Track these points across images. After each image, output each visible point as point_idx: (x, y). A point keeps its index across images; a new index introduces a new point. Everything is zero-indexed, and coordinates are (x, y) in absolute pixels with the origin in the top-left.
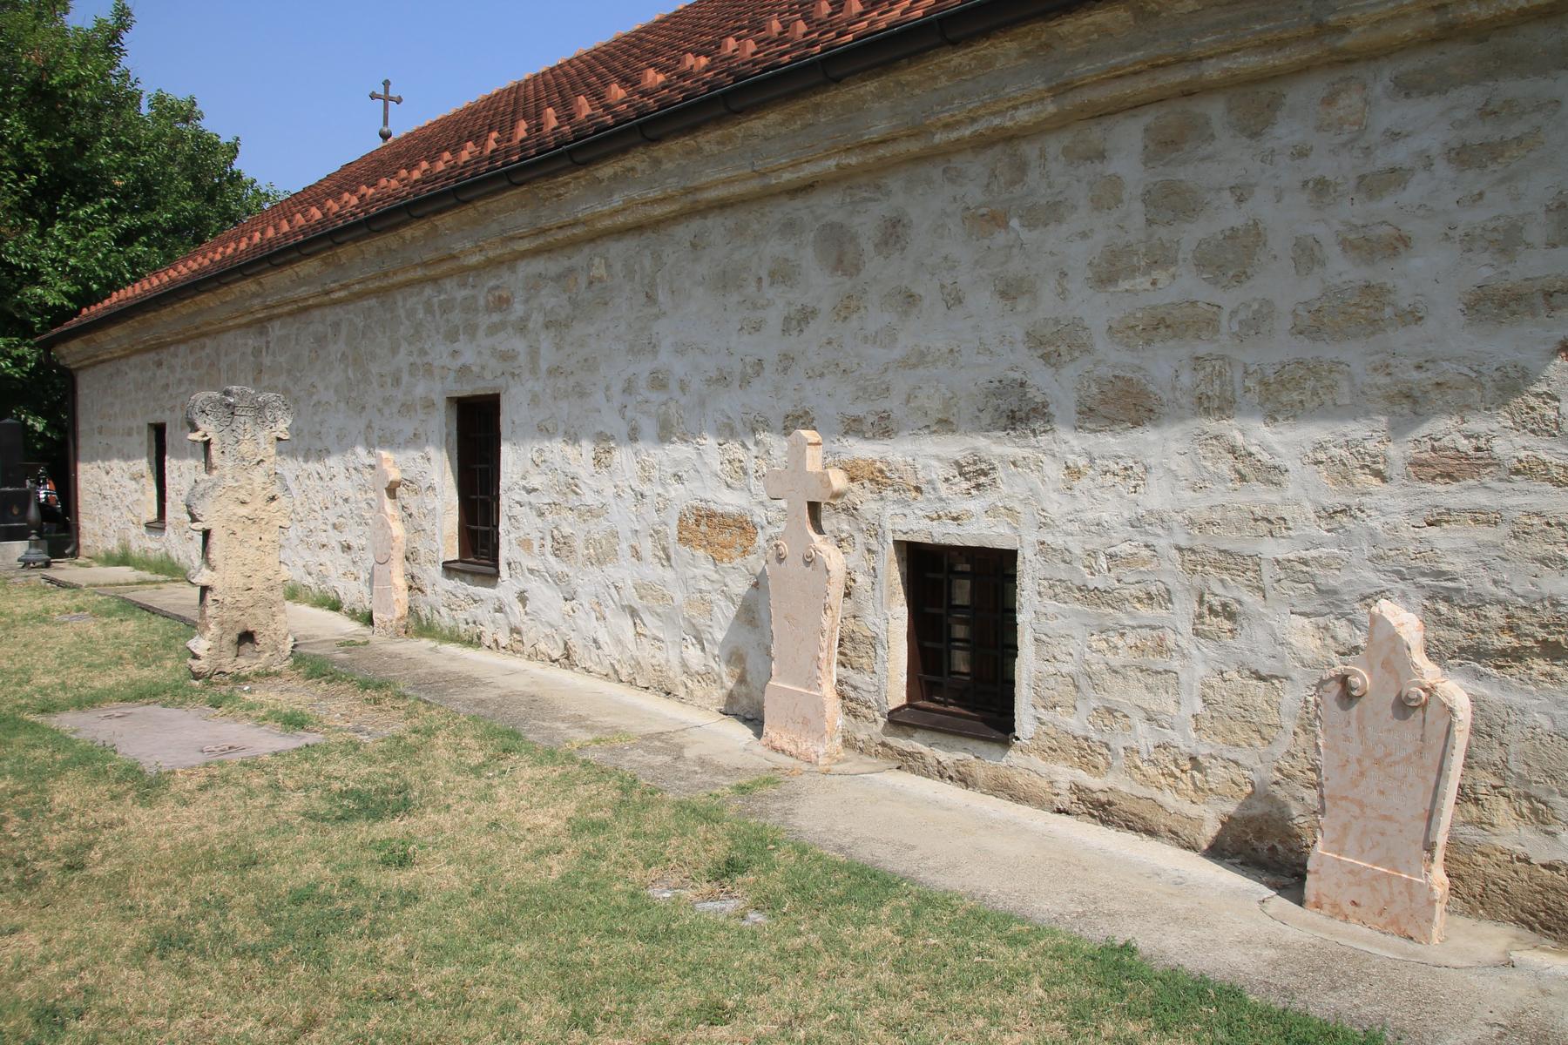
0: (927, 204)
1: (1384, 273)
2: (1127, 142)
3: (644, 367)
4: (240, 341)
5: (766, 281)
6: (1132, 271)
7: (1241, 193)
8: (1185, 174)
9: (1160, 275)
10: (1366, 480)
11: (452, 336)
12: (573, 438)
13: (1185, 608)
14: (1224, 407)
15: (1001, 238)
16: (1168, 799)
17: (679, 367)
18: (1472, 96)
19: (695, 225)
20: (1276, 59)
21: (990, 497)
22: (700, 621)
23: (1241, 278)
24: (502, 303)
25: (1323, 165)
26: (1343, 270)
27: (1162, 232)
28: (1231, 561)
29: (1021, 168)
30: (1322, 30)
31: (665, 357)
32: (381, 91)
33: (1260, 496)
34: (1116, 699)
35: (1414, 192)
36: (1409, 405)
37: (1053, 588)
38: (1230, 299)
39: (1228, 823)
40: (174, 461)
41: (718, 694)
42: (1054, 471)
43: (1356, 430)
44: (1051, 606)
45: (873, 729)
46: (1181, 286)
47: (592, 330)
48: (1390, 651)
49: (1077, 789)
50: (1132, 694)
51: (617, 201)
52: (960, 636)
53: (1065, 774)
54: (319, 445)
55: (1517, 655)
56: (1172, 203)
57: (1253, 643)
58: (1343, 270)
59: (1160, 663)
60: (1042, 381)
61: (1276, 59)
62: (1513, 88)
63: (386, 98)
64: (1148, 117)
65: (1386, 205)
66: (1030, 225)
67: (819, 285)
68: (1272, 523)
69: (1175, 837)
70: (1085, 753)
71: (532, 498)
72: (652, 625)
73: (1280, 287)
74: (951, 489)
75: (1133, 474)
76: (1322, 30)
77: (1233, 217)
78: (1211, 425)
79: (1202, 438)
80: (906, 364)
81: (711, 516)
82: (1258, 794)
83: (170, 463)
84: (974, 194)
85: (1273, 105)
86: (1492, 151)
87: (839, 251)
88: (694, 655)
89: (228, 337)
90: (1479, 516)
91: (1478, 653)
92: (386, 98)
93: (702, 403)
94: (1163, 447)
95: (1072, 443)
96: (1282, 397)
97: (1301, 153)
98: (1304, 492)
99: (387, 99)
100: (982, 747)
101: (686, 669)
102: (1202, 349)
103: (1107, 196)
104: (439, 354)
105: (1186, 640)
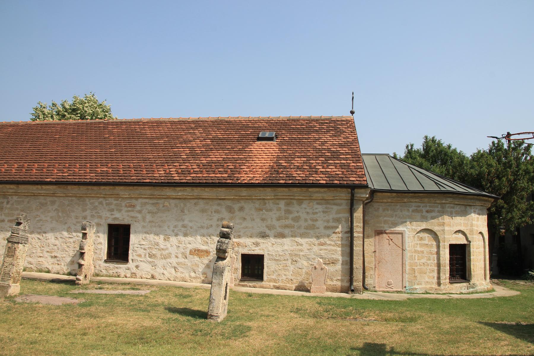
0: (248, 206)
1: (315, 223)
2: (282, 204)
3: (180, 224)
5: (213, 212)
6: (282, 219)
7: (298, 212)
8: (290, 208)
10: (313, 245)
12: (157, 234)
13: (290, 261)
14: (295, 236)
15: (261, 212)
16: (288, 285)
17: (190, 224)
18: (324, 206)
19: (196, 201)
20: (304, 198)
21: (259, 247)
22: (195, 268)
23: (298, 222)
25: (308, 210)
26: (310, 222)
27: (287, 215)
29: (265, 204)
30: (310, 196)
31: (186, 222)
35: (318, 215)
36: (318, 237)
38: (296, 224)
41: (199, 280)
43: (311, 240)
44: (270, 262)
45: (237, 282)
46: (289, 222)
47: (115, 202)
49: (274, 286)
51: (180, 194)
52: (253, 267)
53: (272, 284)
54: (39, 231)
55: (329, 264)
56: (288, 212)
57: (299, 265)
58: (310, 222)
59: (286, 268)
60: (268, 232)
61: (304, 198)
62: (328, 206)
64: (285, 201)
65: (315, 216)
66: (267, 211)
68: (301, 250)
69: (289, 289)
70: (275, 281)
71: (142, 246)
72: (181, 269)
73: (302, 223)
75: (282, 245)
76: (310, 196)
77: (296, 214)
78: (293, 239)
79: (292, 240)
80: (243, 228)
81: (198, 250)
82: (301, 282)
83: (365, 240)
84: (257, 206)
85: (302, 203)
87: (230, 210)
88: (193, 274)
93: (196, 231)
94: (287, 241)
95: (273, 240)
96: (302, 236)
98: (305, 247)
101: (190, 276)
102: (292, 230)
103: (279, 209)
104: (105, 214)
105: (290, 265)
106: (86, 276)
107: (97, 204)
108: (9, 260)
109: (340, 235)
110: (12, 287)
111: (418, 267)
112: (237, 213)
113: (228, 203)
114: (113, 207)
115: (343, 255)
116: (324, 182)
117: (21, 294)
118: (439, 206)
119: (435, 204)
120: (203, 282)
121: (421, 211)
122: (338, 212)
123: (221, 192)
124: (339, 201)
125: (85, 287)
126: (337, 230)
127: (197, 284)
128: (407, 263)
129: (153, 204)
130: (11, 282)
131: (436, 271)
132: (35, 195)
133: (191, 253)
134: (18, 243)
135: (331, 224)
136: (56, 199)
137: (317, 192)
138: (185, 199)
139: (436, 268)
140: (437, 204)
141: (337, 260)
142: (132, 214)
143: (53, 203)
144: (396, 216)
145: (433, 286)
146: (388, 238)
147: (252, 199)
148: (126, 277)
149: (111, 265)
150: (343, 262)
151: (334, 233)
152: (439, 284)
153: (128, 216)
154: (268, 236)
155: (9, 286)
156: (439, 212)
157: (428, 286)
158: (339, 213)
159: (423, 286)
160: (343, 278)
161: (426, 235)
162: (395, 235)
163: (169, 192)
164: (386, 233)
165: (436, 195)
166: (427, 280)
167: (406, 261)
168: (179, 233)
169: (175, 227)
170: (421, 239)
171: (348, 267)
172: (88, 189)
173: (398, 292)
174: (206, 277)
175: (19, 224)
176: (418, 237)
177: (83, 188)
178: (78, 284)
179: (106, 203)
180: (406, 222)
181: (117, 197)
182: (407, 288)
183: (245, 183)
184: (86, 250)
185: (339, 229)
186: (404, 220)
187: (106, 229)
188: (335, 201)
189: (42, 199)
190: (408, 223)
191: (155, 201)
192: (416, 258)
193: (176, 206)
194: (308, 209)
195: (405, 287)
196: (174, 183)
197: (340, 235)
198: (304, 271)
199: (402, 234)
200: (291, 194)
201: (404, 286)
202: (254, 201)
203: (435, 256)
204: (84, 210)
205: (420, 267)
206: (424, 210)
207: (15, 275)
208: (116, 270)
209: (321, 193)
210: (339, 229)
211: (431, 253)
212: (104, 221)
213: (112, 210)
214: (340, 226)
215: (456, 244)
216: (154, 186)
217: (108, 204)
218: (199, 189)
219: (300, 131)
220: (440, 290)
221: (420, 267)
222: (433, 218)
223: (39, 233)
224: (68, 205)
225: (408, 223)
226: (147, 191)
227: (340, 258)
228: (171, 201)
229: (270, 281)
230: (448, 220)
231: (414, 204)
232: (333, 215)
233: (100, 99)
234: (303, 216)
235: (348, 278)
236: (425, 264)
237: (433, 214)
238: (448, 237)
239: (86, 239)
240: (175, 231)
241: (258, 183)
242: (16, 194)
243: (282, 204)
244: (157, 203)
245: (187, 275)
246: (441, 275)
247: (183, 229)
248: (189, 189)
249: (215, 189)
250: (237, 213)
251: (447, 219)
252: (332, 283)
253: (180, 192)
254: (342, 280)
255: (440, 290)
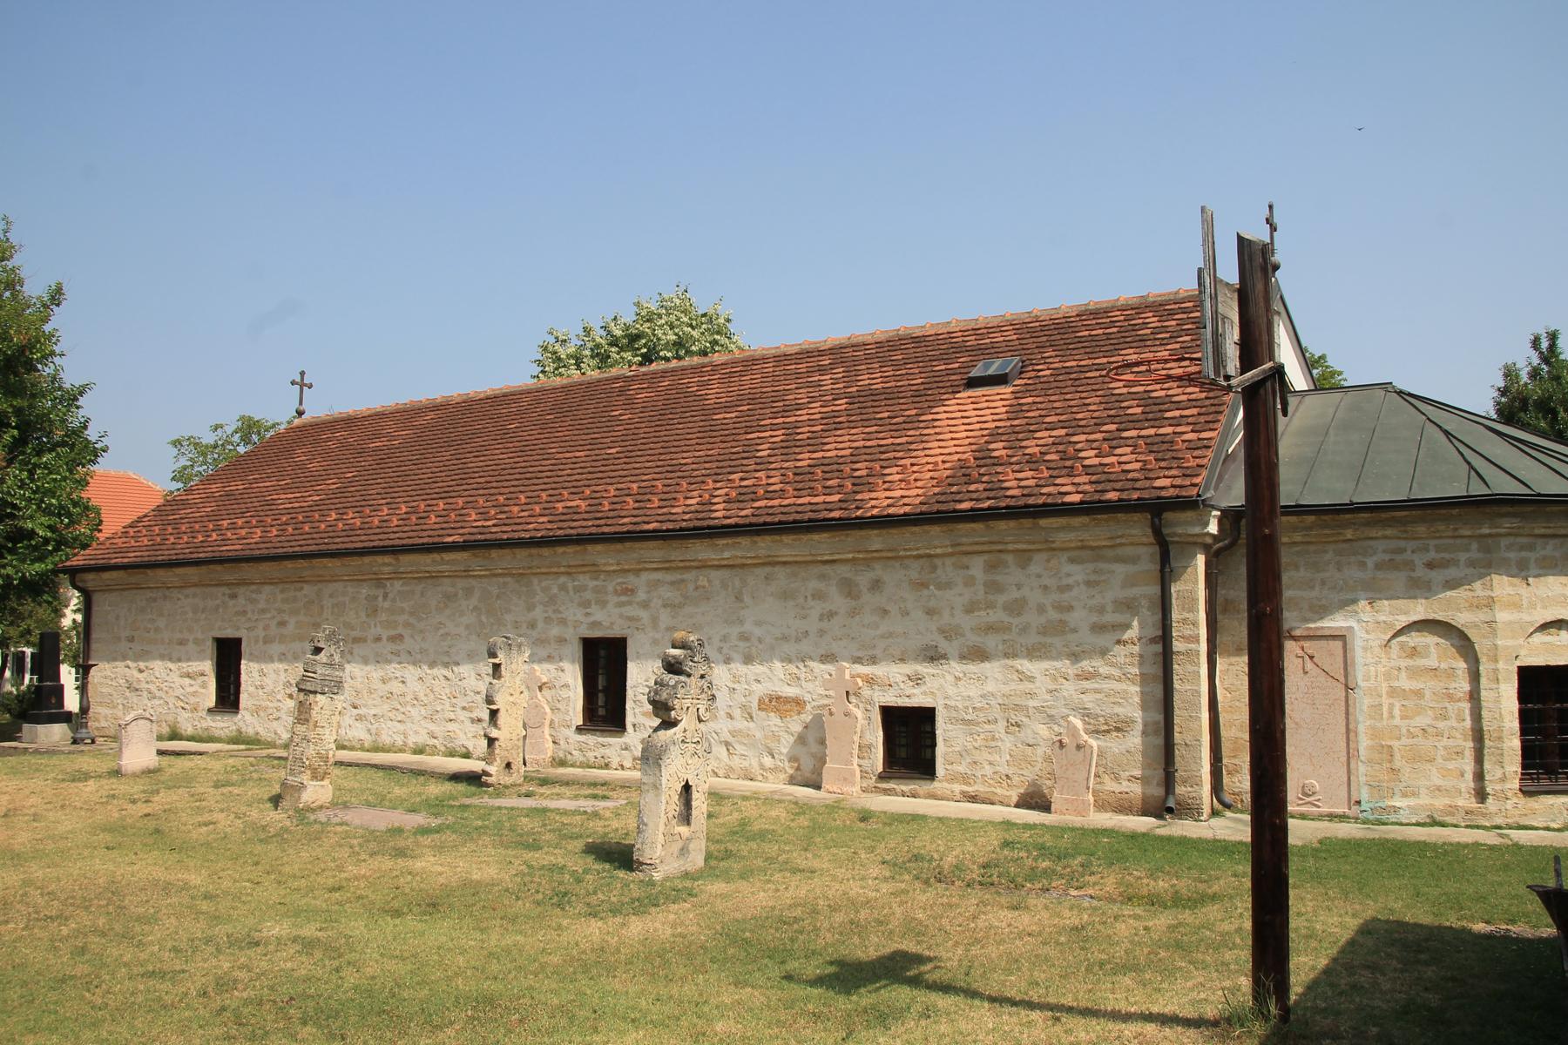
0: (892, 576)
1: (1065, 617)
2: (977, 567)
3: (735, 631)
4: (350, 589)
6: (980, 609)
8: (999, 578)
9: (991, 612)
11: (586, 604)
13: (1002, 724)
14: (1015, 656)
15: (926, 592)
16: (999, 791)
17: (757, 632)
18: (1090, 566)
19: (768, 569)
21: (924, 688)
22: (772, 745)
23: (1019, 614)
24: (630, 591)
25: (1046, 581)
26: (1053, 615)
27: (990, 597)
28: (1017, 707)
29: (934, 568)
31: (748, 627)
32: (298, 379)
33: (1027, 686)
34: (977, 758)
35: (1075, 592)
36: (1075, 657)
37: (951, 721)
38: (1015, 621)
39: (1021, 796)
40: (254, 666)
41: (782, 776)
42: (950, 678)
43: (1058, 664)
44: (950, 727)
45: (872, 781)
46: (997, 616)
47: (592, 584)
48: (1073, 731)
49: (963, 793)
50: (984, 756)
51: (726, 555)
52: (910, 740)
53: (958, 788)
54: (446, 659)
55: (1108, 731)
56: (994, 587)
58: (1053, 615)
60: (944, 646)
63: (302, 384)
64: (986, 557)
65: (1066, 596)
67: (838, 602)
68: (1031, 695)
69: (1001, 803)
70: (965, 779)
72: (740, 749)
73: (1032, 618)
74: (902, 685)
77: (1016, 594)
78: (1010, 662)
79: (1006, 667)
80: (882, 637)
81: (778, 698)
82: (1034, 784)
84: (914, 575)
85: (1030, 559)
86: (1097, 583)
87: (849, 588)
88: (768, 761)
89: (339, 586)
90: (1097, 691)
91: (1097, 732)
92: (302, 384)
93: (773, 648)
94: (992, 669)
95: (956, 667)
96: (1034, 653)
97: (1039, 576)
98: (1042, 685)
99: (302, 385)
100: (922, 782)
101: (762, 767)
103: (970, 582)
104: (573, 613)
106: (508, 765)
107: (555, 590)
108: (301, 729)
109: (1136, 649)
110: (310, 790)
111: (1404, 741)
112: (867, 597)
113: (844, 571)
114: (588, 595)
115: (1144, 707)
116: (1076, 498)
117: (334, 804)
118: (1475, 546)
119: (1458, 541)
120: (792, 781)
121: (1410, 565)
122: (1129, 582)
123: (821, 543)
124: (1129, 551)
125: (502, 790)
126: (1128, 635)
127: (775, 785)
128: (1361, 728)
129: (672, 583)
130: (305, 778)
131: (1469, 755)
132: (434, 577)
133: (762, 705)
134: (315, 692)
135: (1110, 618)
136: (473, 582)
137: (1062, 528)
138: (743, 566)
139: (1470, 744)
140: (1465, 541)
141: (1129, 722)
142: (629, 611)
143: (469, 592)
144: (1323, 583)
145: (1460, 802)
146: (1300, 653)
147: (902, 558)
148: (622, 767)
149: (590, 739)
150: (1145, 725)
151: (1118, 642)
152: (1481, 795)
153: (621, 616)
154: (944, 657)
155: (302, 786)
156: (1472, 564)
157: (1440, 802)
158: (1133, 585)
159: (1424, 800)
160: (1148, 772)
161: (1429, 640)
162: (1323, 643)
163: (701, 551)
164: (1294, 638)
165: (1455, 512)
166: (1437, 780)
167: (1357, 722)
168: (735, 655)
169: (724, 639)
170: (1414, 652)
171: (1160, 741)
172: (531, 555)
173: (1332, 817)
174: (798, 769)
175: (318, 650)
176: (1402, 646)
177: (522, 553)
178: (488, 785)
179: (574, 588)
180: (1354, 601)
181: (595, 570)
182: (1364, 806)
183: (873, 517)
184: (501, 702)
185: (1133, 633)
186: (1349, 596)
187: (576, 650)
188: (1119, 551)
189: (447, 586)
190: (1363, 603)
191: (677, 576)
192: (1397, 712)
193: (724, 586)
194: (1050, 577)
195: (1358, 803)
196: (709, 527)
197: (1136, 649)
198: (1040, 751)
199: (1342, 638)
200: (995, 538)
201: (1354, 798)
202: (906, 561)
203: (1466, 706)
204: (531, 608)
205: (1410, 741)
206: (1419, 560)
207: (317, 762)
208: (602, 750)
209: (1074, 529)
210: (1133, 633)
211: (1450, 698)
212: (571, 630)
213: (586, 604)
214: (1135, 623)
215: (1548, 667)
216: (664, 538)
217: (577, 590)
218: (768, 538)
219: (1093, 346)
220: (1484, 815)
221: (1410, 741)
222: (1451, 585)
223: (446, 665)
224: (498, 597)
225: (1363, 603)
226: (653, 552)
227: (1138, 715)
228: (714, 574)
229: (952, 779)
230: (1510, 590)
231: (1381, 545)
232: (1115, 592)
233: (702, 304)
234: (1034, 597)
235: (1160, 773)
236: (1430, 730)
237: (1452, 572)
238: (1510, 643)
239: (500, 677)
240: (725, 651)
241: (905, 514)
242: (397, 575)
243: (977, 567)
244: (683, 581)
245: (755, 763)
246: (1487, 766)
247: (741, 644)
248: (744, 541)
249: (805, 537)
250: (867, 597)
251: (1503, 586)
252: (1117, 788)
253: (726, 550)
254: (1144, 780)
255: (1484, 815)
